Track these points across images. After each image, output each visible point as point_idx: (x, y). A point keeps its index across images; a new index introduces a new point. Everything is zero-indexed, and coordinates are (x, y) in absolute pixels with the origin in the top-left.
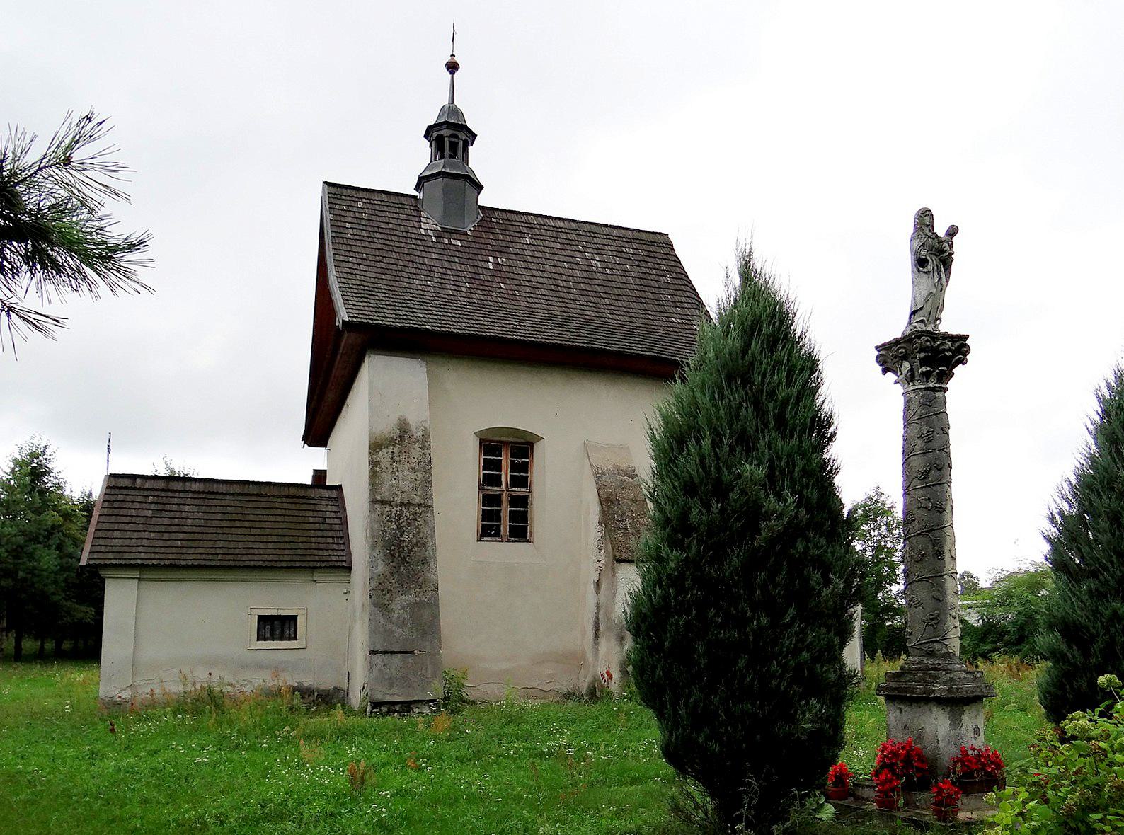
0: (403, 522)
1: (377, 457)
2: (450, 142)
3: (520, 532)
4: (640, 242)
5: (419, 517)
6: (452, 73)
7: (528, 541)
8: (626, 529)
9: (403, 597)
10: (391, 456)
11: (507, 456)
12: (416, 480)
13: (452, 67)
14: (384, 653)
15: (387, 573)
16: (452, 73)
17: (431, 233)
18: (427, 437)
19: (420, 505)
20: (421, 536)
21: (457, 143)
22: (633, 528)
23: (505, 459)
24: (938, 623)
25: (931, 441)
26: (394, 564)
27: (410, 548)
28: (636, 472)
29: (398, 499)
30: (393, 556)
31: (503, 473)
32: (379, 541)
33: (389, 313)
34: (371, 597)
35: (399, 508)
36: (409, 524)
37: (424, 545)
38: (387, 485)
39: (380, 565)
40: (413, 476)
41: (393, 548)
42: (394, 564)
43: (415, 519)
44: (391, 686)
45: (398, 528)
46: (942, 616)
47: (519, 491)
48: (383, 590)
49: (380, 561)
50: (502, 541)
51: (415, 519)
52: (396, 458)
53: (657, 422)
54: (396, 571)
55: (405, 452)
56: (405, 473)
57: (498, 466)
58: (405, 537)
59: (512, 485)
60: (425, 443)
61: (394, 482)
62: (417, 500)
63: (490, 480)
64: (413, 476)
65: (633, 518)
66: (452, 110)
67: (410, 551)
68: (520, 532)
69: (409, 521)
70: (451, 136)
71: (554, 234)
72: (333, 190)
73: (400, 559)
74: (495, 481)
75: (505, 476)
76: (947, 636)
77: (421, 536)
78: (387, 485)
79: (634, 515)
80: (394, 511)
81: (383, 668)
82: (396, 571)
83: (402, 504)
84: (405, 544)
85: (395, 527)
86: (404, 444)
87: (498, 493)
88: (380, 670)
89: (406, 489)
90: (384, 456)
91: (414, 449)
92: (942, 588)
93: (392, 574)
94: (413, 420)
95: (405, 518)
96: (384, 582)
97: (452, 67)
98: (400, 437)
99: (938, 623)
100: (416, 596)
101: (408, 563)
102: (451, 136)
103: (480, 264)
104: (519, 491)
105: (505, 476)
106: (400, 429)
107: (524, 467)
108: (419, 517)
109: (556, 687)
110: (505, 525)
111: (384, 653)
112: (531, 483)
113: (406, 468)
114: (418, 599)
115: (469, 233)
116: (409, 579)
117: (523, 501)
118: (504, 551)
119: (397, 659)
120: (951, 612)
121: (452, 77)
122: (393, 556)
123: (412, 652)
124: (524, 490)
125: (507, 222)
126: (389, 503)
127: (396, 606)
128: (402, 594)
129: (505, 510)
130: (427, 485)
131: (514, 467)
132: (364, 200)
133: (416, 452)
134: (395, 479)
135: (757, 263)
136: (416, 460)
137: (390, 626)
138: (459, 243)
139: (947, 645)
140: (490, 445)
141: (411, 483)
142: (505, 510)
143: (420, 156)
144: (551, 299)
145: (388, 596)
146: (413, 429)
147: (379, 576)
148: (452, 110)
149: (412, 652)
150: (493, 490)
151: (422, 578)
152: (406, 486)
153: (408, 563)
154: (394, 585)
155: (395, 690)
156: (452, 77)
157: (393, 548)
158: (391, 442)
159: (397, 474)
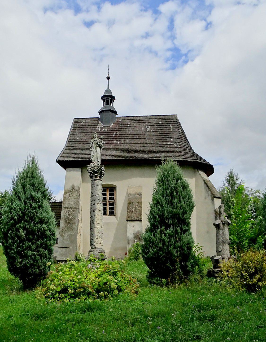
2: (106, 100)
4: (165, 119)
6: (108, 80)
7: (114, 215)
9: (68, 233)
13: (108, 78)
14: (61, 248)
16: (108, 80)
17: (99, 128)
18: (79, 189)
19: (75, 208)
21: (108, 100)
23: (108, 193)
26: (66, 224)
29: (69, 207)
30: (66, 222)
31: (107, 197)
33: (73, 156)
36: (71, 213)
38: (67, 203)
40: (74, 200)
42: (66, 224)
43: (73, 212)
44: (62, 256)
47: (112, 201)
51: (73, 212)
52: (70, 196)
53: (157, 179)
56: (72, 199)
58: (70, 217)
60: (79, 191)
61: (69, 202)
62: (74, 207)
66: (108, 91)
70: (108, 98)
71: (137, 122)
72: (76, 120)
75: (108, 197)
78: (67, 203)
80: (68, 210)
83: (70, 208)
85: (68, 214)
87: (105, 202)
88: (60, 252)
90: (67, 195)
94: (76, 185)
97: (108, 78)
102: (108, 98)
103: (111, 135)
104: (112, 201)
105: (108, 197)
107: (113, 194)
110: (108, 211)
111: (61, 248)
112: (115, 199)
116: (70, 228)
117: (112, 204)
119: (64, 249)
121: (108, 81)
122: (66, 222)
123: (68, 247)
124: (113, 201)
125: (124, 120)
126: (67, 208)
129: (108, 207)
132: (84, 122)
133: (76, 193)
135: (36, 158)
138: (107, 130)
142: (108, 207)
143: (100, 105)
146: (76, 187)
148: (108, 91)
149: (68, 247)
152: (72, 203)
155: (63, 258)
156: (108, 81)
158: (70, 191)
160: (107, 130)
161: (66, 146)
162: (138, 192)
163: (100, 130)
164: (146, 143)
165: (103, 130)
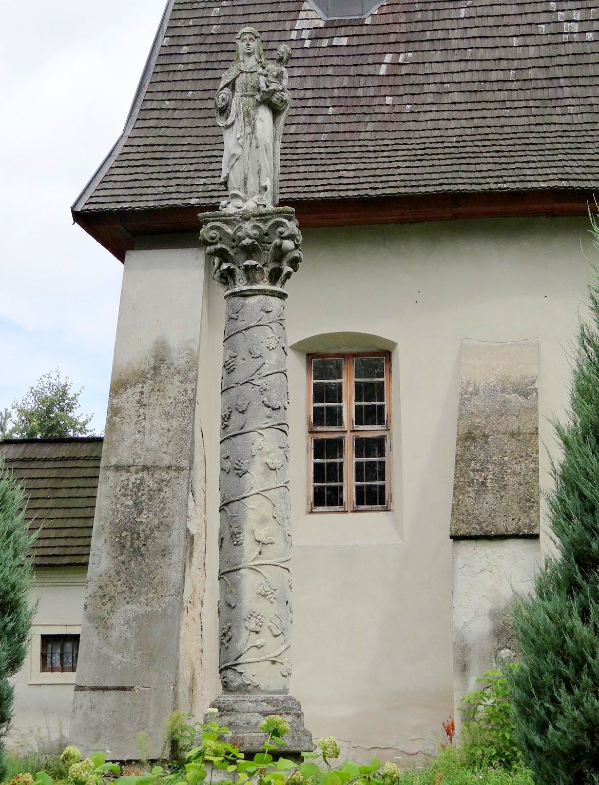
0: (142, 495)
1: (120, 401)
3: (373, 496)
5: (166, 485)
7: (387, 510)
8: (483, 484)
9: (129, 607)
10: (138, 398)
11: (352, 376)
12: (169, 430)
14: (94, 689)
15: (113, 573)
17: (305, 34)
20: (165, 514)
22: (497, 481)
24: (230, 639)
25: (232, 371)
26: (123, 558)
27: (148, 532)
28: (536, 385)
29: (140, 462)
30: (123, 547)
31: (344, 404)
32: (107, 525)
34: (86, 607)
35: (140, 474)
36: (151, 498)
37: (168, 527)
39: (103, 560)
40: (165, 425)
41: (124, 534)
42: (123, 558)
43: (160, 490)
45: (136, 504)
46: (234, 630)
48: (103, 597)
49: (104, 555)
50: (346, 512)
51: (160, 490)
52: (145, 401)
54: (124, 567)
55: (159, 390)
56: (155, 422)
57: (335, 394)
58: (143, 518)
59: (359, 421)
61: (137, 436)
63: (325, 416)
64: (165, 425)
65: (502, 464)
67: (147, 537)
68: (373, 496)
69: (151, 493)
73: (131, 549)
74: (334, 417)
75: (348, 406)
76: (240, 660)
77: (165, 514)
78: (127, 442)
79: (506, 459)
80: (132, 480)
81: (89, 711)
82: (124, 567)
83: (145, 468)
84: (142, 527)
85: (130, 503)
86: (158, 379)
89: (153, 444)
90: (129, 398)
91: (172, 384)
92: (236, 588)
93: (118, 573)
94: (175, 341)
95: (147, 489)
96: (106, 585)
98: (155, 368)
99: (230, 639)
100: (147, 605)
101: (142, 555)
104: (371, 431)
105: (348, 406)
106: (156, 357)
108: (166, 485)
109: (426, 747)
110: (349, 485)
111: (94, 689)
113: (157, 413)
114: (149, 609)
115: (368, 21)
117: (373, 447)
118: (351, 526)
120: (247, 624)
123: (131, 689)
126: (127, 468)
127: (117, 620)
128: (128, 603)
129: (349, 460)
130: (184, 436)
131: (362, 391)
133: (174, 388)
134: (139, 432)
136: (171, 400)
137: (105, 650)
139: (241, 673)
140: (322, 360)
141: (162, 435)
142: (349, 460)
144: (469, 106)
145: (109, 605)
146: (174, 355)
147: (101, 576)
150: (328, 432)
151: (159, 577)
152: (153, 440)
153: (142, 555)
154: (119, 589)
157: (124, 534)
158: (142, 377)
159: (143, 424)
160: (344, 41)
161: (129, 133)
162: (518, 374)
163: (307, 44)
164: (559, 103)
165: (325, 43)
